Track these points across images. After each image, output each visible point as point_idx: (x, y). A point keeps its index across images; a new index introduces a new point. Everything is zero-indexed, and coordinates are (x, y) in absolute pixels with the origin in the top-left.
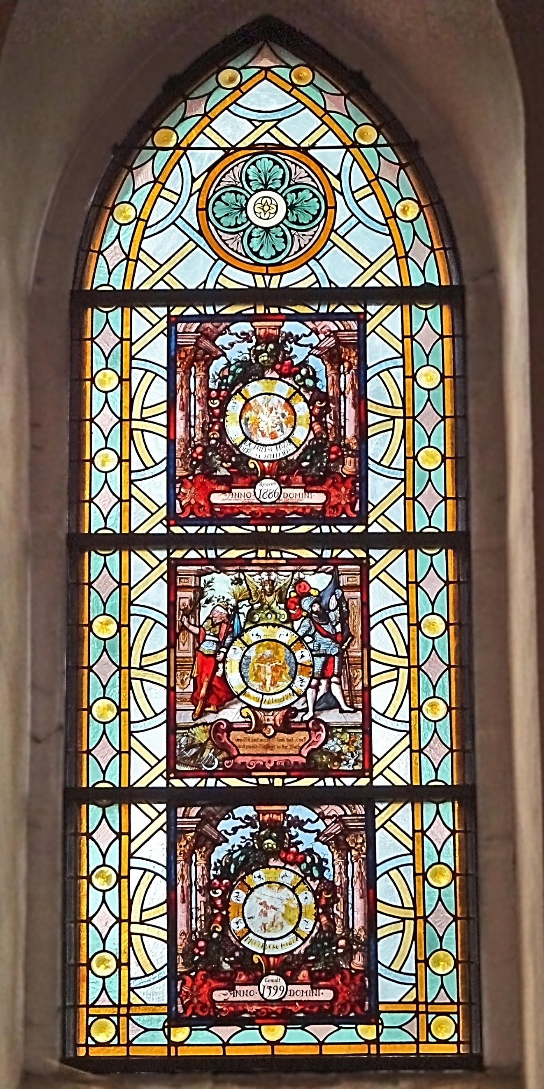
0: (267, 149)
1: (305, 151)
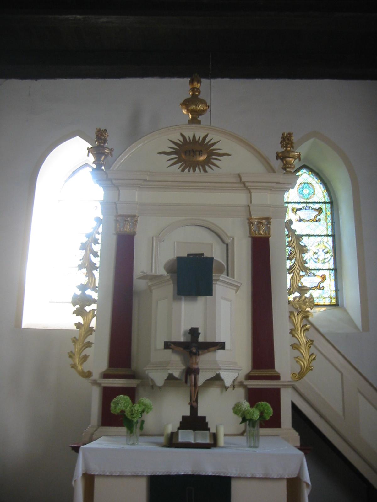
0: (306, 183)
1: (311, 183)
